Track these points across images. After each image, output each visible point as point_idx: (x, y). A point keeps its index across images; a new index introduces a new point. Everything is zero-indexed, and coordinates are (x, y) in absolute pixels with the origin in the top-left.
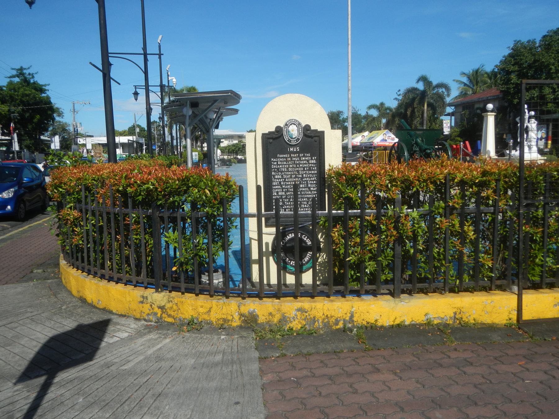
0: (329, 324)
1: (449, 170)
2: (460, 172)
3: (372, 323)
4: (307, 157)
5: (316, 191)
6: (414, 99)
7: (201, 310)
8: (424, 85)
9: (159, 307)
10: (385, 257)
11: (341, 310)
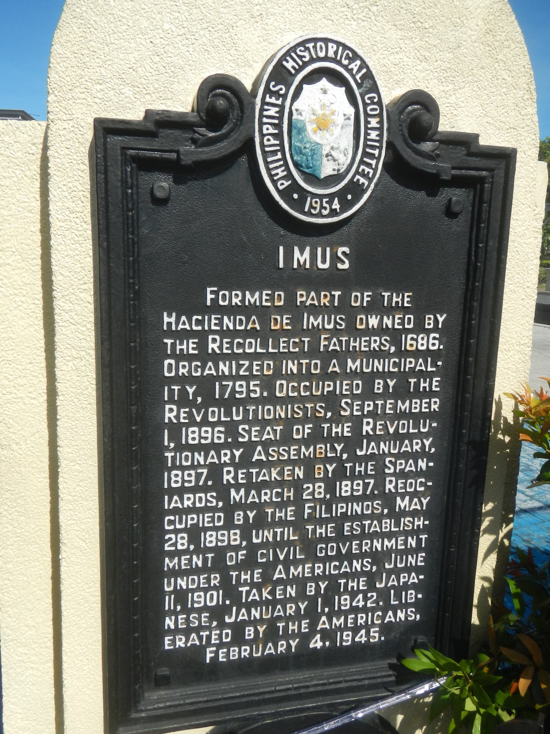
4: (390, 310)
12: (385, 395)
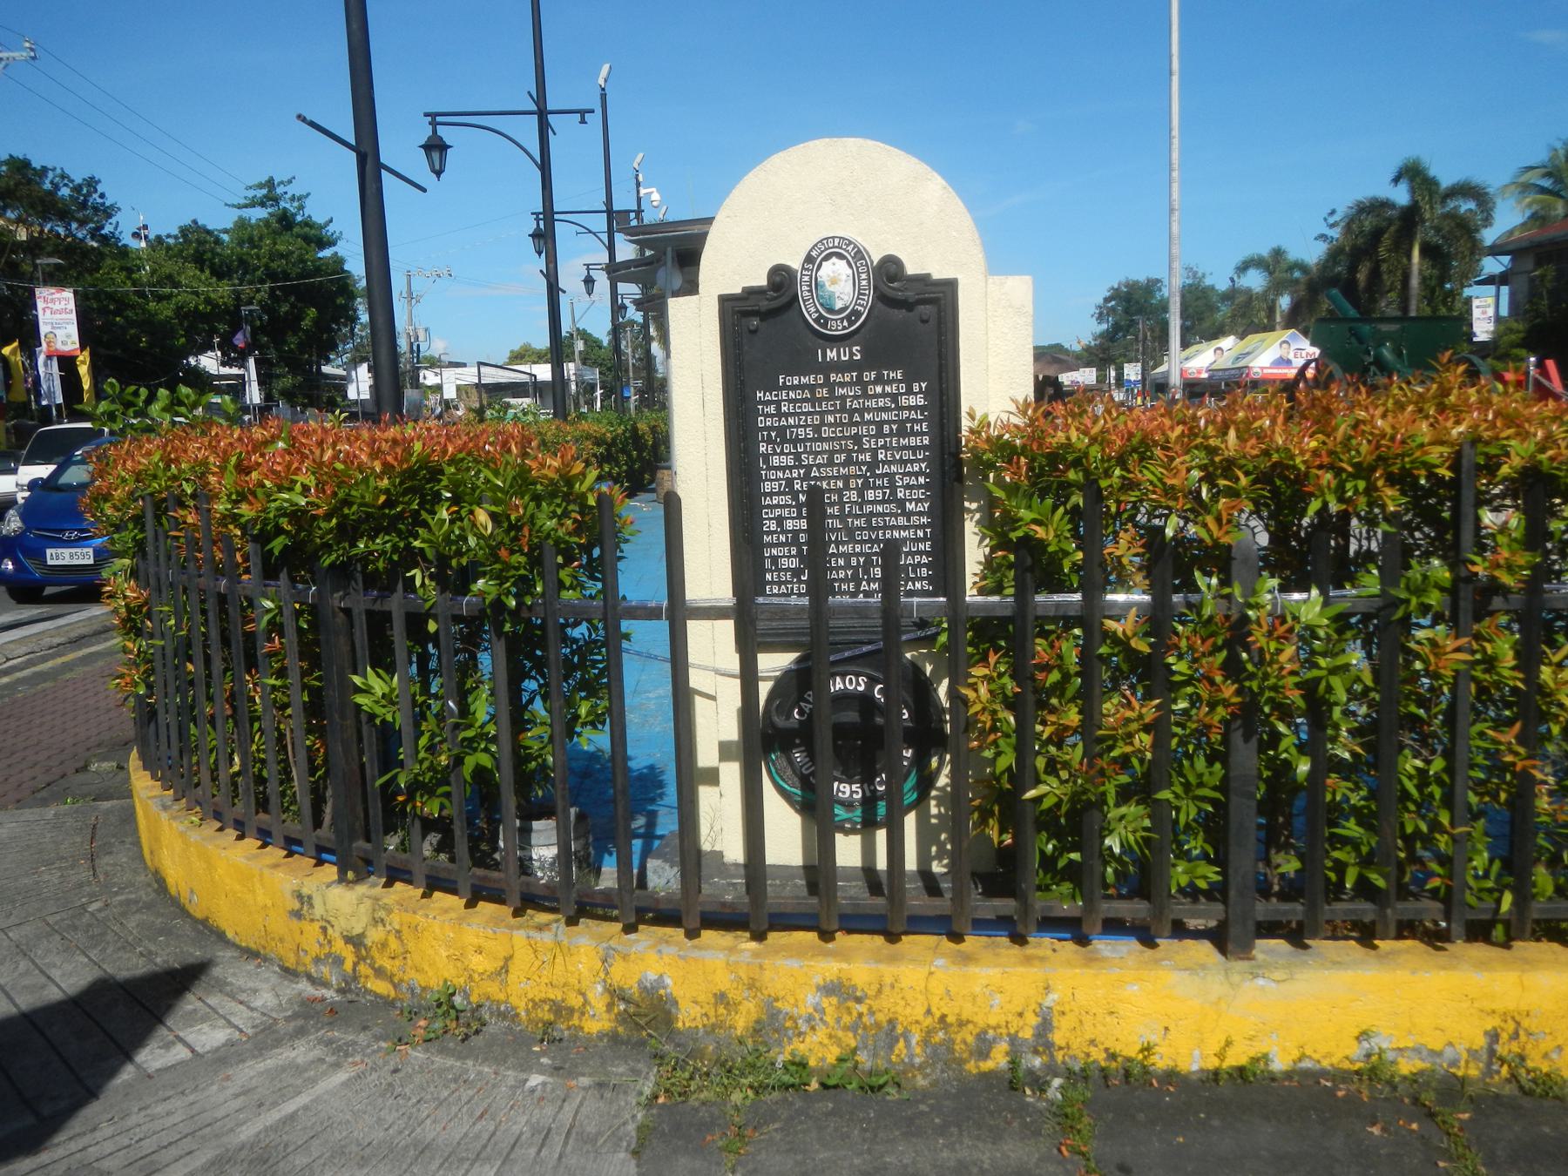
0: (951, 1050)
1: (1476, 427)
2: (1524, 435)
3: (1129, 1060)
4: (890, 382)
5: (928, 514)
6: (1377, 235)
7: (479, 963)
8: (1412, 191)
9: (349, 940)
10: (1187, 787)
11: (998, 999)
12: (891, 434)
